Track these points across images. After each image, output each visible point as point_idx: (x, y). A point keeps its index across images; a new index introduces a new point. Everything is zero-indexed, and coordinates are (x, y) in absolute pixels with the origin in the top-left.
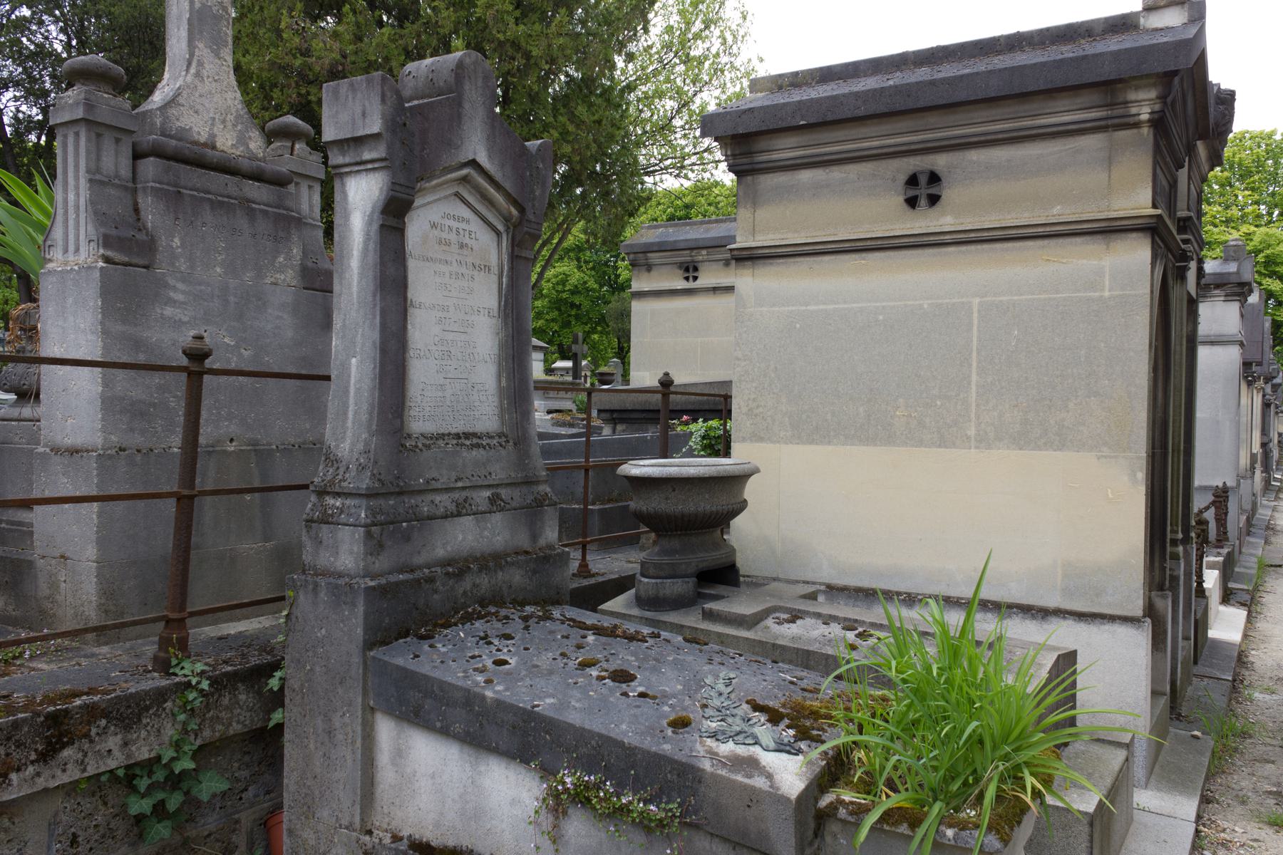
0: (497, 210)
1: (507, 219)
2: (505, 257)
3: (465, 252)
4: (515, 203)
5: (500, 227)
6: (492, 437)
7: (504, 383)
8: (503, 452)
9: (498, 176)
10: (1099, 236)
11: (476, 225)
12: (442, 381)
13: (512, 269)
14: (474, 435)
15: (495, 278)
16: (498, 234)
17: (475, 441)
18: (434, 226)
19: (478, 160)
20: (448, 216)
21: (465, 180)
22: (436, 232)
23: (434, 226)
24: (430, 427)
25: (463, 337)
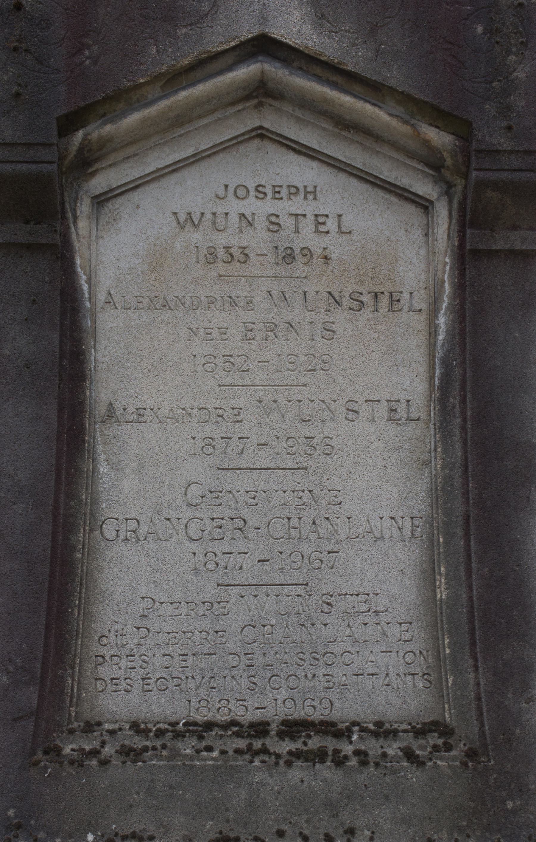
0: (395, 145)
1: (432, 163)
2: (445, 262)
3: (300, 268)
4: (440, 117)
5: (425, 188)
6: (393, 734)
7: (442, 594)
8: (414, 776)
9: (356, 58)
10: (381, 193)
11: (338, 197)
12: (211, 592)
13: (460, 288)
14: (328, 728)
15: (418, 322)
16: (425, 206)
17: (315, 743)
18: (190, 221)
19: (280, 31)
20: (240, 192)
21: (261, 93)
22: (195, 237)
23: (190, 221)
24: (164, 707)
25: (292, 480)
